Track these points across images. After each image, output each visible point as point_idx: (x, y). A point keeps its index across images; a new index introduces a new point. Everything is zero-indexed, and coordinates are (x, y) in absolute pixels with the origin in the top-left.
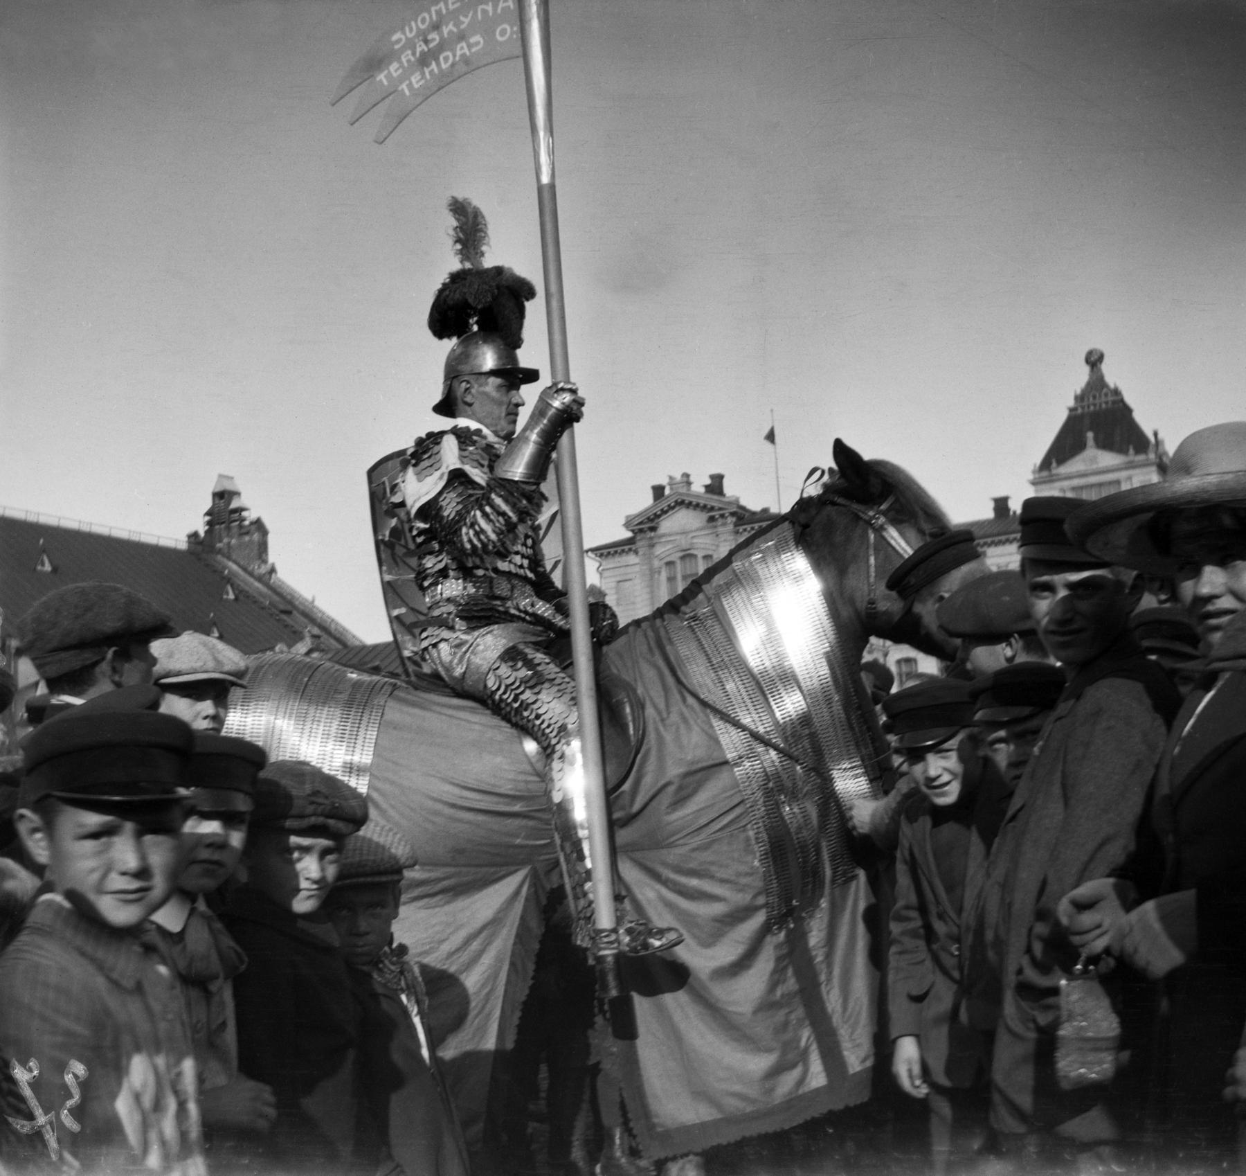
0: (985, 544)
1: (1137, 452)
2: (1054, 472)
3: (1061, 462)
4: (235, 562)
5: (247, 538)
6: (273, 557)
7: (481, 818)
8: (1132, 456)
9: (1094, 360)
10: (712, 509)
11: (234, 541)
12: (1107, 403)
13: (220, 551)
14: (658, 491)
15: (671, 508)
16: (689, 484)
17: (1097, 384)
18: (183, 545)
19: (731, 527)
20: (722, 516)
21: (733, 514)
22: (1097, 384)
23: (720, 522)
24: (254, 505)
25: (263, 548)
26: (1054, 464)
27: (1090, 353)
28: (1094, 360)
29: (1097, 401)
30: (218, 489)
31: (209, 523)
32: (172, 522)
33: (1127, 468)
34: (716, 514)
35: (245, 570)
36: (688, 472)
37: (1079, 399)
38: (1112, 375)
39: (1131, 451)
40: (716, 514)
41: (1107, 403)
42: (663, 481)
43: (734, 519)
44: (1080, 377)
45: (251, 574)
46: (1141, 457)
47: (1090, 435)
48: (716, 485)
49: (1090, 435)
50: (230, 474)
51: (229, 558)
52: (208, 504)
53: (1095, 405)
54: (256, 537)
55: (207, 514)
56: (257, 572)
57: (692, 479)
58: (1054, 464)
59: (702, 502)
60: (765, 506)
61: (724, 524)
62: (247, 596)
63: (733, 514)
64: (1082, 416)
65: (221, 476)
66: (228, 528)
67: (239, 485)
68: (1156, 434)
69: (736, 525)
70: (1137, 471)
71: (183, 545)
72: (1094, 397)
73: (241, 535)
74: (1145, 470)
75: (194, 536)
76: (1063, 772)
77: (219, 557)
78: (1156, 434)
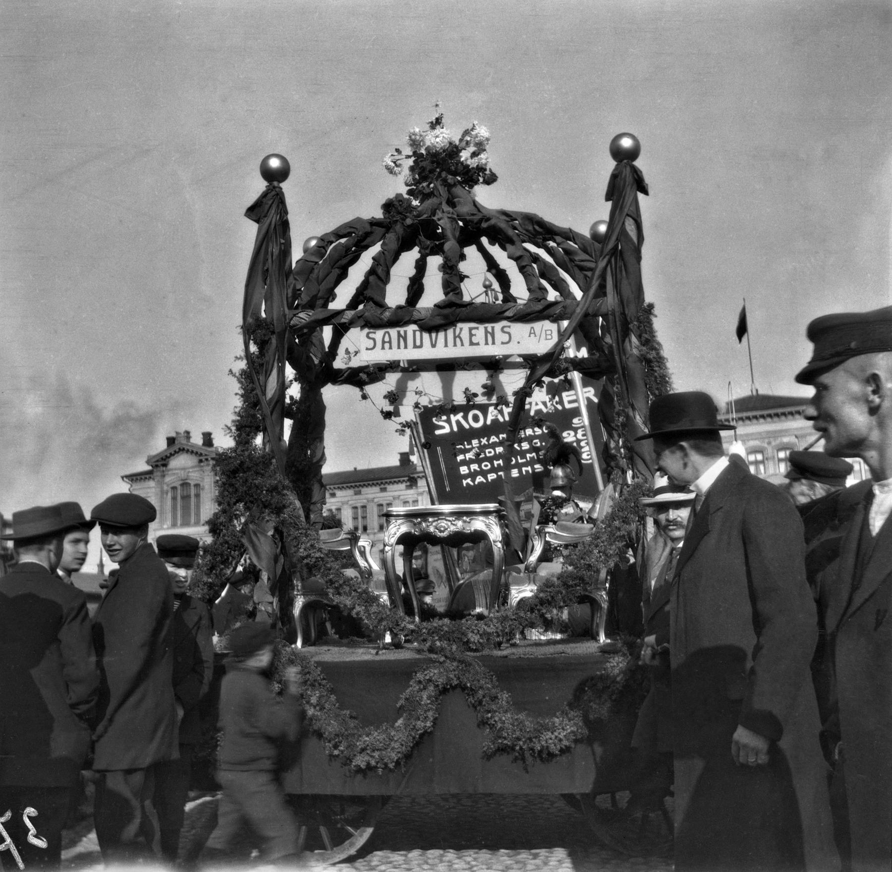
10: (201, 455)
14: (171, 441)
15: (176, 452)
20: (207, 460)
21: (213, 459)
23: (206, 463)
34: (203, 458)
36: (188, 429)
40: (203, 458)
42: (173, 435)
57: (191, 434)
59: (199, 451)
61: (208, 465)
63: (213, 459)
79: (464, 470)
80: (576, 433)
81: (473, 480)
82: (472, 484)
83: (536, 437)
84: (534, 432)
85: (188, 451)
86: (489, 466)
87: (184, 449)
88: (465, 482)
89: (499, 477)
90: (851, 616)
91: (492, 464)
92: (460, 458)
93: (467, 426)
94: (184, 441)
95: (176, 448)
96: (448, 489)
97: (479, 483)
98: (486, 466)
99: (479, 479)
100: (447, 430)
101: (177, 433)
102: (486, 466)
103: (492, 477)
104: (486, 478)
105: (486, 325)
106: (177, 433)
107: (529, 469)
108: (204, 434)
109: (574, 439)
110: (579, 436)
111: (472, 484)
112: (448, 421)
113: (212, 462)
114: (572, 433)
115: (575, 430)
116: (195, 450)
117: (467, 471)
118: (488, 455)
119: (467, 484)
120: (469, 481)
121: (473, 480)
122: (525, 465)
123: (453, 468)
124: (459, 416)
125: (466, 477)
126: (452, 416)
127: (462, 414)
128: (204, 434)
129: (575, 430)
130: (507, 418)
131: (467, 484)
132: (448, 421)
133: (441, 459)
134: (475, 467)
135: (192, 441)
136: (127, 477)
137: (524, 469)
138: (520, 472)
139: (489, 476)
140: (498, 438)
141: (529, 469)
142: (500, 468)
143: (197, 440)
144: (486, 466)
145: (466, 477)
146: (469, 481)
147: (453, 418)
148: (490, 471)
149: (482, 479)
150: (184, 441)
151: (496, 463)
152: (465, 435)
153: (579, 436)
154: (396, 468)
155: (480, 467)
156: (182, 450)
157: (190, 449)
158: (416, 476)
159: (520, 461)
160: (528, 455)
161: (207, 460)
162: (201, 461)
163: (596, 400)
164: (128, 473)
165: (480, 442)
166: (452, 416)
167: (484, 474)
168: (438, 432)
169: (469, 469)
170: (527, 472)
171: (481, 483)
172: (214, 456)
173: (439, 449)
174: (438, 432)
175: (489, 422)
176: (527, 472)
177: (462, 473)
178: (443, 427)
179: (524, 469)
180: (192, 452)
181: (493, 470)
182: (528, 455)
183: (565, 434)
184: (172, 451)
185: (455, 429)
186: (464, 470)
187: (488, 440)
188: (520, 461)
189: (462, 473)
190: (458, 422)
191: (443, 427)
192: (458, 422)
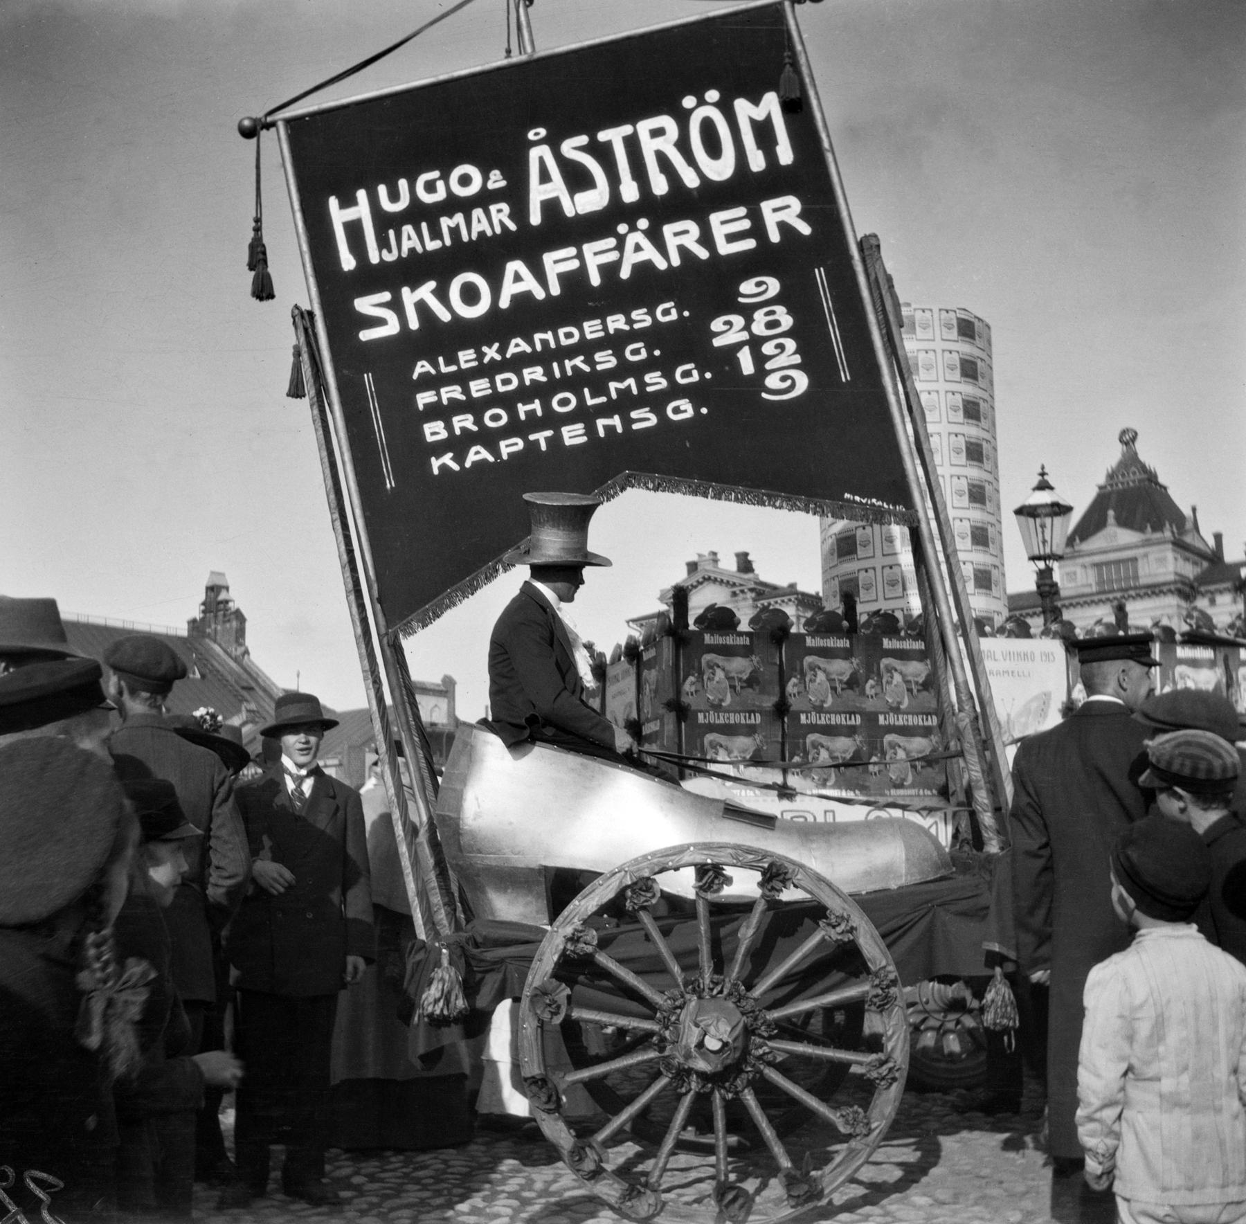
0: (1028, 614)
1: (1154, 529)
2: (1077, 548)
3: (1083, 539)
4: (220, 645)
5: (228, 625)
6: (250, 640)
7: (932, 886)
8: (1150, 534)
9: (1128, 438)
10: (734, 585)
11: (219, 628)
12: (1134, 481)
13: (209, 636)
14: (692, 567)
15: (699, 583)
16: (716, 561)
17: (1131, 461)
18: (183, 631)
19: (751, 602)
20: (742, 591)
21: (752, 590)
22: (1131, 461)
23: (741, 595)
24: (238, 598)
25: (240, 633)
26: (1078, 540)
27: (1124, 432)
28: (1128, 438)
29: (1127, 479)
30: (210, 584)
31: (204, 612)
32: (169, 614)
33: (1143, 546)
34: (737, 589)
35: (225, 651)
36: (715, 550)
37: (1111, 476)
38: (1147, 454)
39: (1149, 529)
40: (737, 589)
41: (1134, 481)
42: (695, 558)
43: (753, 595)
44: (1113, 455)
45: (229, 655)
46: (1158, 535)
47: (1111, 513)
48: (745, 564)
49: (1111, 513)
50: (221, 571)
51: (215, 641)
52: (202, 597)
53: (1122, 483)
54: (234, 624)
55: (203, 604)
56: (233, 654)
57: (719, 556)
58: (1078, 540)
59: (732, 580)
60: (792, 581)
61: (745, 599)
62: (221, 679)
63: (752, 590)
64: (1110, 493)
65: (212, 573)
66: (216, 616)
67: (230, 582)
68: (1194, 510)
69: (755, 600)
70: (1155, 548)
71: (183, 631)
72: (1123, 475)
73: (224, 622)
74: (1162, 547)
75: (193, 622)
76: (1050, 909)
77: (207, 640)
78: (1194, 510)
79: (434, 431)
80: (749, 321)
81: (460, 458)
82: (455, 467)
83: (633, 336)
84: (630, 322)
85: (715, 580)
86: (505, 419)
87: (709, 578)
88: (435, 464)
89: (532, 446)
90: (220, 805)
91: (513, 413)
92: (424, 399)
93: (445, 316)
94: (710, 567)
95: (698, 576)
96: (390, 484)
97: (474, 464)
98: (496, 418)
99: (478, 454)
100: (392, 328)
101: (700, 555)
102: (496, 418)
103: (510, 447)
104: (495, 451)
105: (524, 58)
106: (700, 555)
107: (616, 421)
108: (738, 555)
109: (745, 336)
110: (759, 328)
111: (455, 467)
112: (396, 305)
113: (750, 595)
114: (738, 321)
115: (747, 312)
116: (725, 579)
117: (444, 435)
118: (501, 389)
119: (443, 468)
120: (447, 459)
121: (460, 458)
122: (605, 410)
123: (407, 422)
124: (426, 291)
125: (439, 449)
126: (405, 291)
127: (432, 284)
128: (738, 555)
129: (747, 312)
130: (555, 290)
131: (443, 468)
132: (396, 305)
133: (374, 406)
134: (464, 422)
135: (721, 565)
136: (634, 621)
137: (601, 423)
138: (591, 430)
139: (502, 444)
140: (531, 342)
141: (616, 421)
142: (534, 423)
143: (729, 564)
144: (496, 418)
145: (439, 449)
146: (447, 459)
147: (409, 297)
148: (506, 432)
149: (485, 455)
150: (710, 567)
151: (522, 409)
152: (438, 338)
153: (759, 328)
154: (1030, 594)
155: (478, 421)
156: (707, 579)
157: (719, 577)
158: (1059, 604)
159: (590, 402)
160: (613, 386)
161: (742, 591)
162: (734, 594)
163: (805, 229)
164: (635, 616)
165: (480, 355)
166: (405, 291)
167: (489, 439)
168: (366, 335)
169: (449, 427)
170: (610, 429)
171: (480, 465)
172: (752, 586)
173: (368, 378)
174: (366, 335)
175: (504, 303)
176: (610, 429)
177: (430, 439)
178: (381, 322)
179: (601, 423)
180: (715, 580)
181: (515, 428)
182: (613, 386)
183: (717, 325)
184: (693, 581)
185: (414, 324)
186: (434, 431)
187: (502, 351)
188: (590, 402)
189: (430, 439)
190: (421, 307)
191: (381, 322)
192: (421, 307)
